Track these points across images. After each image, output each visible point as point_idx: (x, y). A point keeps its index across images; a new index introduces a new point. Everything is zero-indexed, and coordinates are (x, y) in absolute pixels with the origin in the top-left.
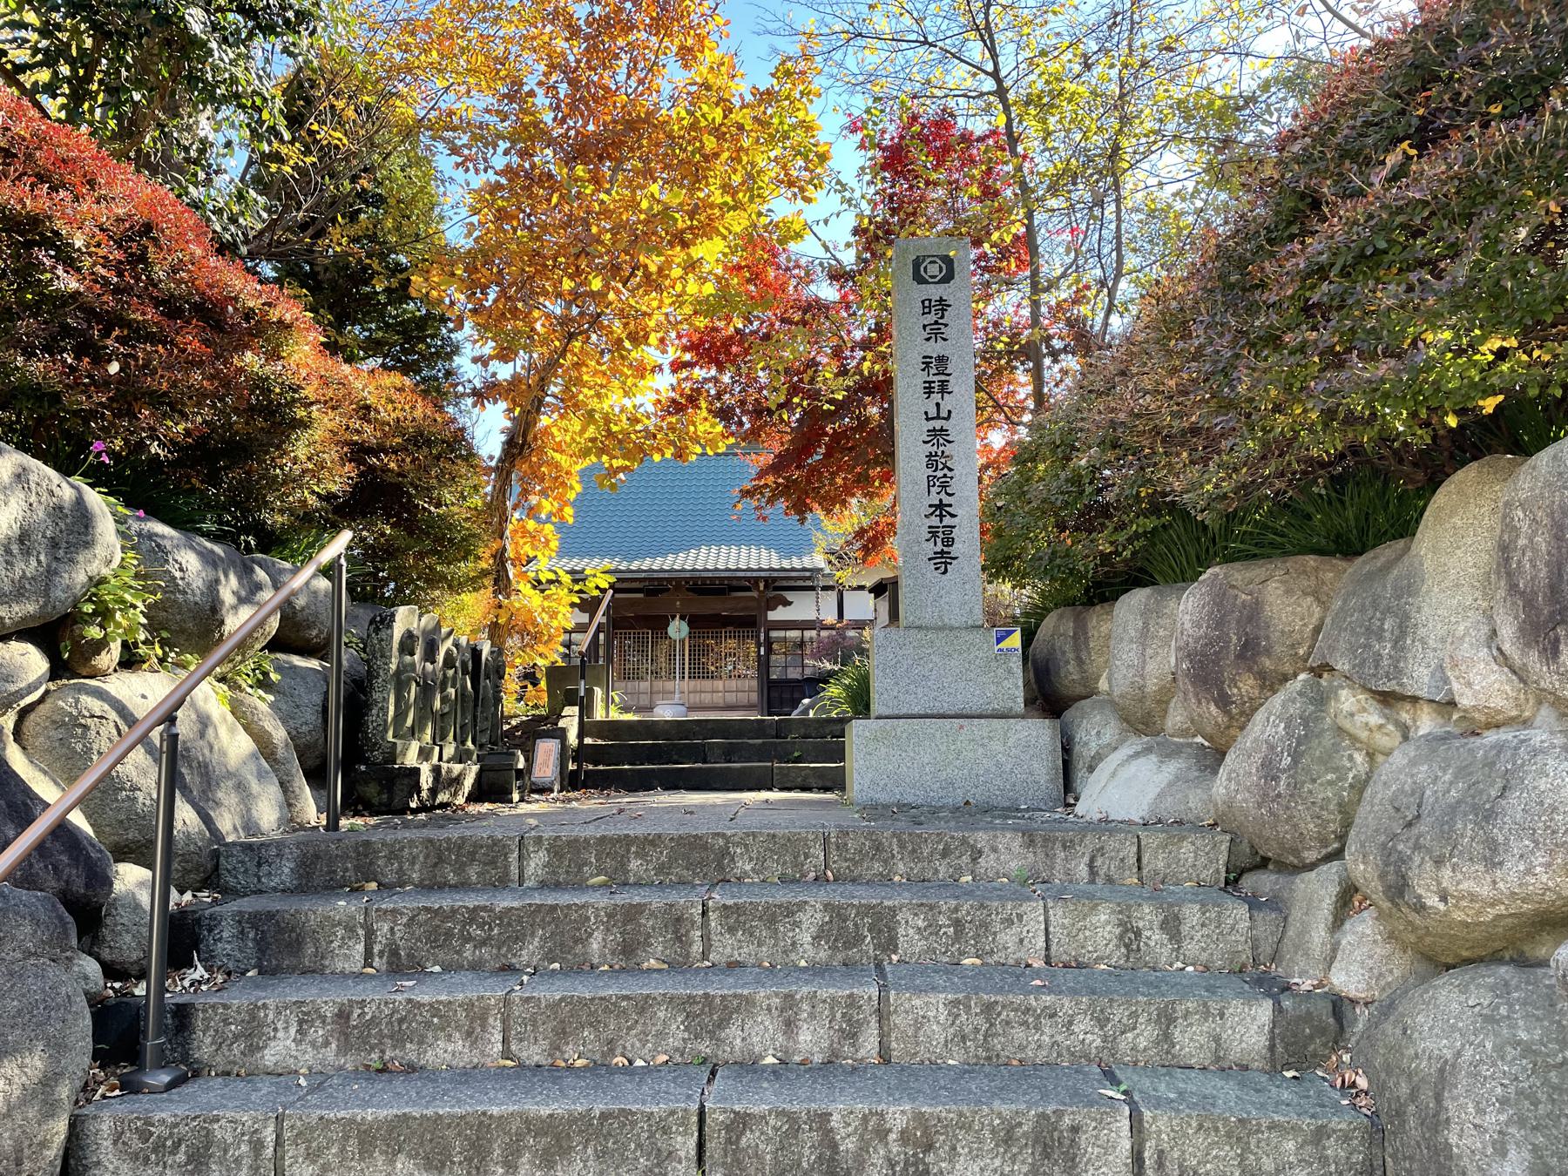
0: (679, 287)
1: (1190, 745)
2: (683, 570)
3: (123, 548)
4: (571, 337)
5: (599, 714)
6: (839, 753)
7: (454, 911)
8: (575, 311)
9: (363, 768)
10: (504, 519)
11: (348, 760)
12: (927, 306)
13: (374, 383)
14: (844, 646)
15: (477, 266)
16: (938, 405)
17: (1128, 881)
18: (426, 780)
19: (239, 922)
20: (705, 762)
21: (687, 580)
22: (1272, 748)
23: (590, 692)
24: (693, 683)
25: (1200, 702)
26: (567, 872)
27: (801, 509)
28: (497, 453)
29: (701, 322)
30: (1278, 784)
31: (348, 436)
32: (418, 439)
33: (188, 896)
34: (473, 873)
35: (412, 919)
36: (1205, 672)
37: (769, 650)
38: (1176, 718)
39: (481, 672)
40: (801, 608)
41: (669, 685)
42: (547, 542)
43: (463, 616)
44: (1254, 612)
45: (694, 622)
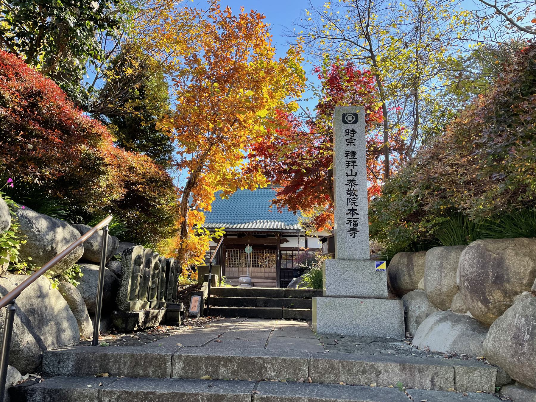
0: (251, 127)
1: (464, 317)
2: (251, 229)
3: (12, 222)
4: (212, 144)
5: (217, 286)
6: (310, 305)
7: (138, 394)
8: (215, 136)
9: (116, 312)
10: (186, 210)
11: (111, 310)
12: (347, 132)
13: (140, 161)
14: (308, 259)
15: (180, 119)
16: (351, 170)
17: (450, 389)
18: (141, 317)
19: (44, 393)
20: (256, 306)
21: (252, 232)
22: (519, 329)
23: (213, 277)
24: (253, 269)
25: (473, 301)
26: (192, 372)
27: (294, 208)
28: (185, 185)
29: (260, 140)
30: (523, 348)
31: (124, 178)
32: (152, 180)
33: (26, 377)
34: (150, 371)
35: (119, 396)
36: (476, 288)
37: (281, 258)
38: (457, 303)
39: (170, 271)
40: (292, 243)
41: (245, 269)
42: (201, 218)
43: (166, 248)
44: (500, 263)
45: (255, 247)
